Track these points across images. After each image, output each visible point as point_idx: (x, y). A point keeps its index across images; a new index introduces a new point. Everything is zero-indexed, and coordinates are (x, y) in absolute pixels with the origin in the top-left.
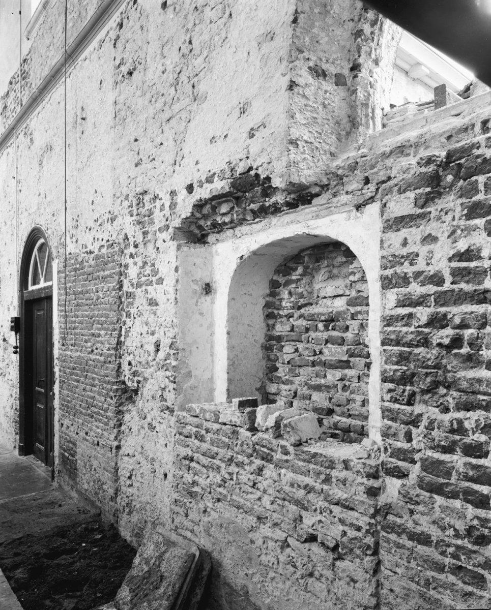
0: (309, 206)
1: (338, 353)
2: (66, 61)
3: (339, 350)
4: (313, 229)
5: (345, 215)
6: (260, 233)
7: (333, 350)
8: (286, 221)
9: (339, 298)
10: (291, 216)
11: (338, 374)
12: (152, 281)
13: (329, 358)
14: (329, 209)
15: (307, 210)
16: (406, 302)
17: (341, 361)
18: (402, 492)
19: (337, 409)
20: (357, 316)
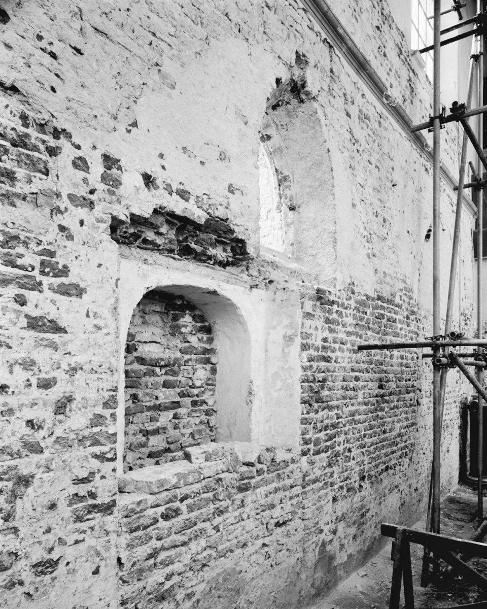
0: (222, 269)
1: (171, 396)
2: (349, 49)
3: (172, 393)
4: (222, 289)
5: (242, 289)
6: (177, 272)
7: (167, 393)
8: (203, 272)
9: (154, 344)
10: (219, 272)
11: (171, 414)
12: (40, 284)
13: (163, 401)
14: (237, 281)
15: (221, 272)
16: (311, 360)
17: (173, 402)
18: (292, 467)
19: (172, 446)
20: (188, 362)
